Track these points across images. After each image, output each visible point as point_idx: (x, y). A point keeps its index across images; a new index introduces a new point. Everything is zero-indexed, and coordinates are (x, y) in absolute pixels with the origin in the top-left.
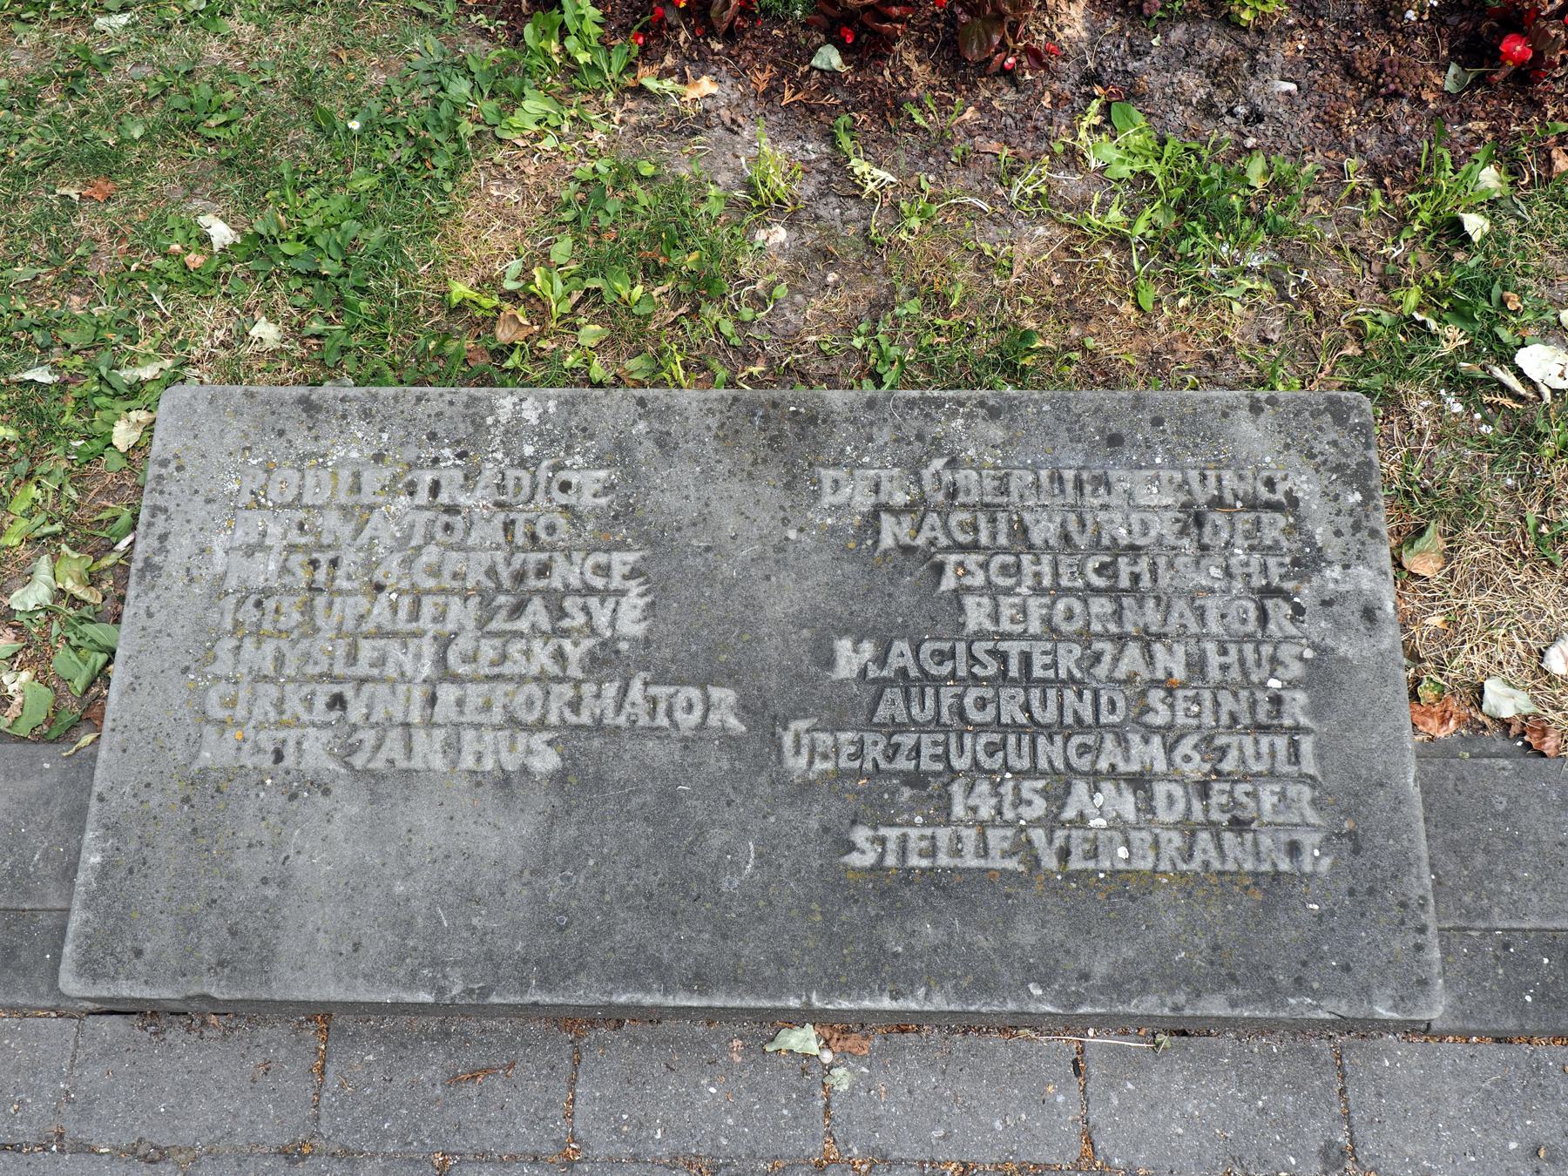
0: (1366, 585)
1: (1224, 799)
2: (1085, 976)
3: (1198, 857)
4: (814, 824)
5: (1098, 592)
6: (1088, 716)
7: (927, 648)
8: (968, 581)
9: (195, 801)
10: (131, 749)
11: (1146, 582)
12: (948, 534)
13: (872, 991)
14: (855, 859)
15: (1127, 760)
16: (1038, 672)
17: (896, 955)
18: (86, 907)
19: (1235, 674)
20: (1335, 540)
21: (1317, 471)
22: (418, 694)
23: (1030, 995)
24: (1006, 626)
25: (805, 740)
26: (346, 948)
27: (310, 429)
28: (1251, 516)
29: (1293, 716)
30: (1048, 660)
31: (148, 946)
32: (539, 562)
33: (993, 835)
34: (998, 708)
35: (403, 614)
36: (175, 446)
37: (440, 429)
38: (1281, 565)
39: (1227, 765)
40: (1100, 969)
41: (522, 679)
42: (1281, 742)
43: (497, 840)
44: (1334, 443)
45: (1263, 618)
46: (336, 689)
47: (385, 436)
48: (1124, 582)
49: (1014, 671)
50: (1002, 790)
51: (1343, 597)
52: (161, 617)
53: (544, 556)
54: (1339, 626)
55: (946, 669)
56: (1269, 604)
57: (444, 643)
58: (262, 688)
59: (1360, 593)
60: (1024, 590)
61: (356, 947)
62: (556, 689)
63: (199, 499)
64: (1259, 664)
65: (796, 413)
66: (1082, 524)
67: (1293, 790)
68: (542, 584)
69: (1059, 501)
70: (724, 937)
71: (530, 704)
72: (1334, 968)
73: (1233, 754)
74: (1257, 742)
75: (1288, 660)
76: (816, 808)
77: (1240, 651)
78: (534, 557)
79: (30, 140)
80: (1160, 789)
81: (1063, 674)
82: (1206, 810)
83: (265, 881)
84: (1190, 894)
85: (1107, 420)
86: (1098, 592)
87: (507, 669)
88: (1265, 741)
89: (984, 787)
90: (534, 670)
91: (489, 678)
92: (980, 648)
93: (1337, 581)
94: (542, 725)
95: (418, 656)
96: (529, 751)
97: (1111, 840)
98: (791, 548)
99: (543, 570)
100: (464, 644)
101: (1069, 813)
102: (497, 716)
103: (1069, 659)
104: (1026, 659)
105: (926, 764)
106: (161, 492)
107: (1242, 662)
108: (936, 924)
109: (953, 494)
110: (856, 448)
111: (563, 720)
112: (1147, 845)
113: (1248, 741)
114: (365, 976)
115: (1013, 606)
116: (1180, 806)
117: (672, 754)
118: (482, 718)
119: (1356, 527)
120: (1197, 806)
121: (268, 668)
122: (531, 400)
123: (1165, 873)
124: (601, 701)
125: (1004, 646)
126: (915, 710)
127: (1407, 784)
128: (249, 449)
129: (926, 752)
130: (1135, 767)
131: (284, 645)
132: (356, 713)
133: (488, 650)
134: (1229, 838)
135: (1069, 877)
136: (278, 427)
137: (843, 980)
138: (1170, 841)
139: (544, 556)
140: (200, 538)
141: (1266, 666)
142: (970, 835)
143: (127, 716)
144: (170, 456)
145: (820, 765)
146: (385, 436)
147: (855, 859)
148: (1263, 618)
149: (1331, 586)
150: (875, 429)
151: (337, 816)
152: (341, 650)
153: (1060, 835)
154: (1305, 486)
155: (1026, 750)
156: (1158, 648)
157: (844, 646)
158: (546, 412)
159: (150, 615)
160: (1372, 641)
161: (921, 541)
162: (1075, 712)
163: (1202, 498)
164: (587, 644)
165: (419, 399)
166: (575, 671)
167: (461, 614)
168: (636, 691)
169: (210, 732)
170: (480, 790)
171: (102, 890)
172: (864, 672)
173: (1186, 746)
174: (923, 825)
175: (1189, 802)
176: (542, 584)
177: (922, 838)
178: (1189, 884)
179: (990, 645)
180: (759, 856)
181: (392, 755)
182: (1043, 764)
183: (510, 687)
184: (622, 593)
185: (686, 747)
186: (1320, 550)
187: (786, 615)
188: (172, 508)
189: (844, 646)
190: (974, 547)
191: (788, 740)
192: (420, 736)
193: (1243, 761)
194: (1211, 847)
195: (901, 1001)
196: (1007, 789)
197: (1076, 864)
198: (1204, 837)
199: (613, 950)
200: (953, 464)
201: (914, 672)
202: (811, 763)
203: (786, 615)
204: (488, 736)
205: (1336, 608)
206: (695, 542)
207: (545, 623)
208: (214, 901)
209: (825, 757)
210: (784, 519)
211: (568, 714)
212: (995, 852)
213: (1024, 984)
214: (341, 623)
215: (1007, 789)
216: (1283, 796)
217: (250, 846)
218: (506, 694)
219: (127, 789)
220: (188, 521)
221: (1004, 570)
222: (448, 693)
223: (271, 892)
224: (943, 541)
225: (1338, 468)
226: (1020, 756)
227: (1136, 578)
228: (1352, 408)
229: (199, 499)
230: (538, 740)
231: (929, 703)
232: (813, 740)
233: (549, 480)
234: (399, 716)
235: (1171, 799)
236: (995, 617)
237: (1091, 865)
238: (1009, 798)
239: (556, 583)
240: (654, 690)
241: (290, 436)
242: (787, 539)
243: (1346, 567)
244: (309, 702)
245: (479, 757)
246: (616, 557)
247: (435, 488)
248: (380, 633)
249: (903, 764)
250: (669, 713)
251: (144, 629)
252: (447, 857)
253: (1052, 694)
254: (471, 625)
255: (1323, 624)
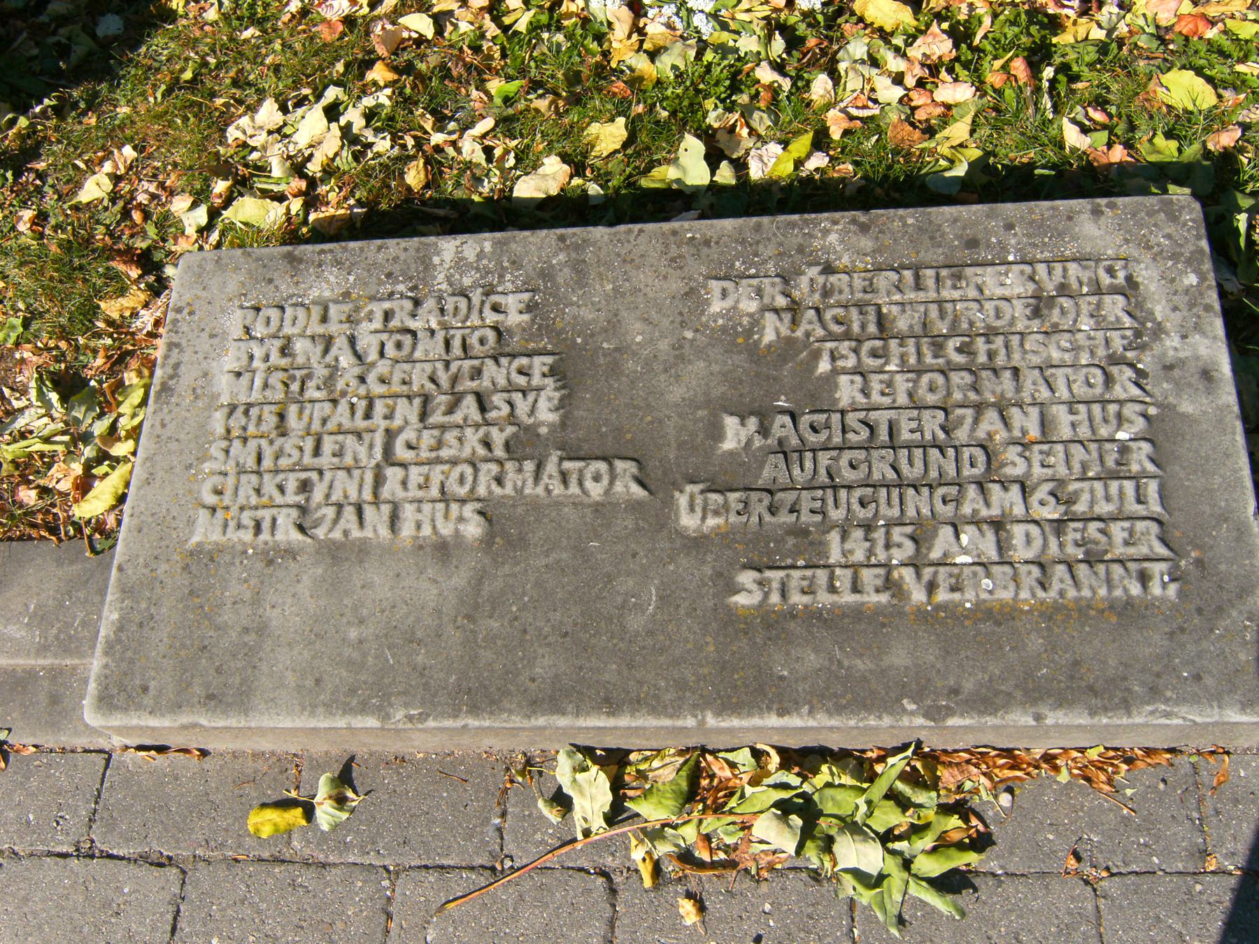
0: (1203, 351)
1: (1078, 536)
2: (955, 691)
3: (1056, 586)
4: (708, 571)
5: (959, 368)
6: (951, 471)
7: (805, 420)
8: (840, 363)
9: (193, 568)
10: (145, 530)
11: (1000, 360)
12: (824, 327)
13: (761, 709)
14: (741, 599)
15: (988, 504)
16: (905, 436)
17: (782, 678)
18: (106, 653)
19: (1084, 432)
20: (1172, 315)
21: (1154, 259)
22: (369, 477)
23: (904, 710)
24: (876, 398)
25: (699, 500)
26: (309, 683)
27: (292, 277)
28: (1094, 299)
29: (1140, 462)
30: (914, 425)
31: (152, 684)
32: (473, 367)
33: (867, 575)
34: (870, 467)
35: (360, 413)
36: (187, 297)
37: (396, 269)
38: (1123, 337)
39: (1080, 507)
40: (968, 686)
41: (454, 462)
42: (1129, 486)
43: (435, 592)
44: (1168, 237)
45: (1109, 380)
46: (304, 475)
47: (352, 278)
48: (982, 358)
49: (883, 436)
50: (875, 535)
51: (1182, 363)
52: (171, 427)
53: (476, 362)
54: (1179, 387)
55: (823, 436)
56: (1114, 370)
57: (390, 435)
58: (244, 478)
59: (1198, 358)
60: (891, 367)
61: (318, 681)
62: (484, 467)
63: (205, 335)
64: (1106, 421)
65: (693, 238)
66: (942, 315)
67: (1140, 526)
68: (474, 385)
69: (921, 296)
70: (630, 666)
71: (462, 480)
72: (1186, 678)
73: (1085, 497)
74: (1106, 487)
75: (1134, 417)
76: (709, 558)
77: (1089, 412)
78: (467, 364)
79: (1167, 630)
80: (1018, 531)
81: (928, 437)
82: (1061, 545)
83: (246, 630)
84: (1050, 618)
85: (964, 229)
86: (959, 368)
87: (445, 453)
88: (1114, 486)
89: (858, 534)
90: (467, 452)
91: (430, 462)
92: (852, 419)
93: (1176, 349)
94: (471, 497)
95: (371, 446)
96: (461, 519)
97: (975, 574)
98: (687, 346)
99: (477, 373)
100: (409, 435)
101: (935, 554)
102: (435, 492)
103: (932, 423)
104: (892, 428)
105: (806, 517)
106: (177, 332)
107: (1090, 419)
108: (816, 651)
109: (826, 293)
110: (744, 263)
111: (490, 492)
112: (1008, 578)
113: (1098, 486)
114: (324, 705)
115: (881, 382)
116: (1038, 543)
117: (584, 517)
118: (420, 494)
119: (1191, 305)
120: (1053, 543)
121: (251, 463)
122: (470, 242)
123: (1026, 600)
124: (519, 478)
125: (873, 415)
126: (796, 471)
127: (1247, 517)
128: (245, 295)
129: (805, 506)
130: (995, 512)
131: (264, 443)
132: (318, 495)
133: (428, 438)
134: (1082, 570)
135: (938, 608)
136: (268, 276)
137: (734, 700)
138: (1029, 573)
139: (476, 362)
140: (204, 364)
141: (1114, 422)
142: (843, 577)
143: (143, 505)
144: (183, 304)
145: (712, 522)
146: (352, 278)
147: (741, 599)
148: (1109, 380)
149: (1171, 353)
150: (761, 247)
151: (305, 577)
152: (309, 444)
153: (928, 572)
154: (1144, 272)
155: (896, 501)
156: (1015, 411)
157: (731, 422)
158: (482, 251)
159: (163, 426)
160: (1211, 397)
161: (799, 333)
162: (940, 467)
163: (1050, 288)
164: (510, 430)
165: (380, 248)
166: (499, 452)
167: (407, 411)
168: (551, 467)
169: (203, 515)
170: (421, 553)
171: (119, 641)
172: (749, 442)
173: (1042, 492)
174: (805, 567)
175: (1045, 539)
176: (474, 385)
177: (803, 578)
178: (1052, 614)
179: (862, 415)
180: (661, 598)
181: (348, 526)
182: (911, 513)
183: (446, 467)
184: (539, 389)
185: (597, 510)
186: (1160, 323)
187: (684, 399)
188: (184, 343)
189: (731, 422)
190: (847, 336)
191: (683, 501)
192: (369, 511)
193: (1092, 502)
194: (1067, 577)
195: (786, 718)
196: (879, 535)
197: (942, 596)
198: (1061, 570)
199: (533, 680)
200: (828, 270)
201: (794, 441)
202: (704, 518)
203: (684, 399)
204: (427, 507)
205: (1176, 373)
206: (605, 345)
207: (476, 416)
208: (205, 647)
209: (716, 513)
210: (683, 322)
211: (494, 487)
212: (870, 589)
213: (898, 700)
214: (310, 424)
215: (879, 535)
216: (1131, 532)
217: (234, 603)
218: (443, 473)
219: (141, 560)
220: (196, 352)
221: (874, 354)
222: (393, 474)
223: (251, 639)
224: (820, 332)
225: (1175, 257)
226: (889, 504)
227: (991, 355)
228: (1183, 207)
229: (205, 335)
230: (469, 510)
231: (808, 464)
232: (705, 501)
233: (483, 303)
234: (353, 496)
235: (1028, 540)
236: (865, 392)
237: (957, 596)
238: (881, 542)
239: (486, 383)
240: (567, 465)
241: (276, 283)
242: (684, 338)
243: (1184, 337)
244: (281, 489)
245: (419, 526)
246: (537, 360)
247: (388, 316)
248: (340, 431)
249: (786, 518)
250: (580, 483)
251: (158, 436)
252: (394, 607)
253: (918, 453)
254: (414, 418)
255: (1165, 385)
